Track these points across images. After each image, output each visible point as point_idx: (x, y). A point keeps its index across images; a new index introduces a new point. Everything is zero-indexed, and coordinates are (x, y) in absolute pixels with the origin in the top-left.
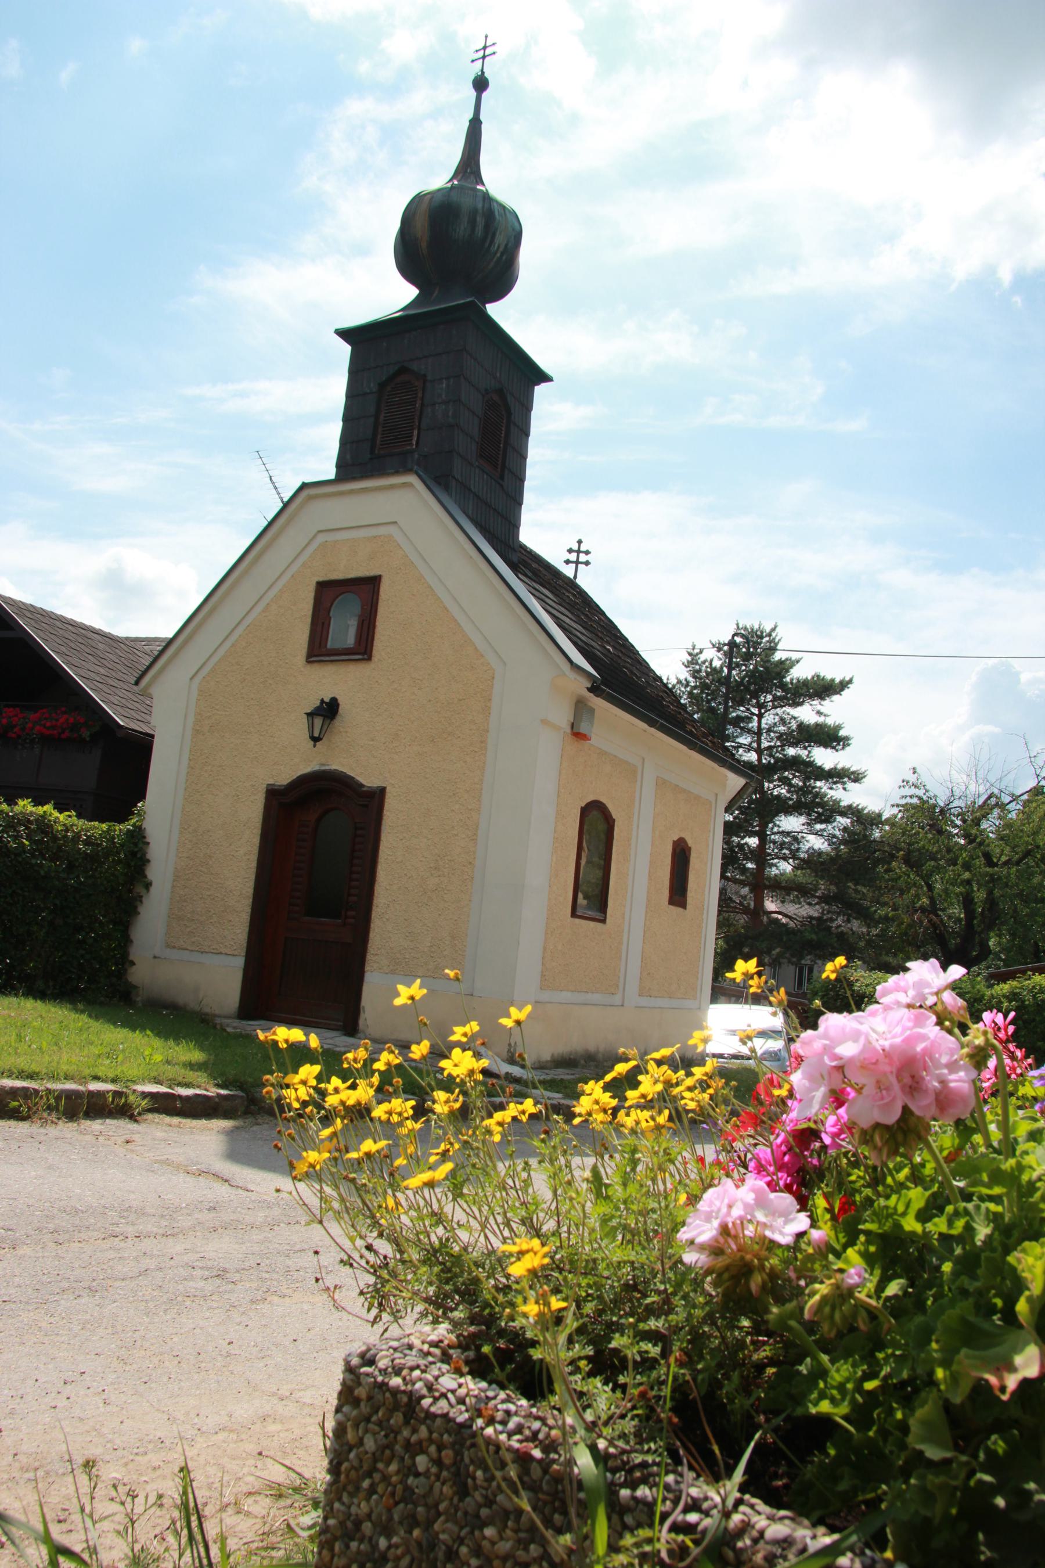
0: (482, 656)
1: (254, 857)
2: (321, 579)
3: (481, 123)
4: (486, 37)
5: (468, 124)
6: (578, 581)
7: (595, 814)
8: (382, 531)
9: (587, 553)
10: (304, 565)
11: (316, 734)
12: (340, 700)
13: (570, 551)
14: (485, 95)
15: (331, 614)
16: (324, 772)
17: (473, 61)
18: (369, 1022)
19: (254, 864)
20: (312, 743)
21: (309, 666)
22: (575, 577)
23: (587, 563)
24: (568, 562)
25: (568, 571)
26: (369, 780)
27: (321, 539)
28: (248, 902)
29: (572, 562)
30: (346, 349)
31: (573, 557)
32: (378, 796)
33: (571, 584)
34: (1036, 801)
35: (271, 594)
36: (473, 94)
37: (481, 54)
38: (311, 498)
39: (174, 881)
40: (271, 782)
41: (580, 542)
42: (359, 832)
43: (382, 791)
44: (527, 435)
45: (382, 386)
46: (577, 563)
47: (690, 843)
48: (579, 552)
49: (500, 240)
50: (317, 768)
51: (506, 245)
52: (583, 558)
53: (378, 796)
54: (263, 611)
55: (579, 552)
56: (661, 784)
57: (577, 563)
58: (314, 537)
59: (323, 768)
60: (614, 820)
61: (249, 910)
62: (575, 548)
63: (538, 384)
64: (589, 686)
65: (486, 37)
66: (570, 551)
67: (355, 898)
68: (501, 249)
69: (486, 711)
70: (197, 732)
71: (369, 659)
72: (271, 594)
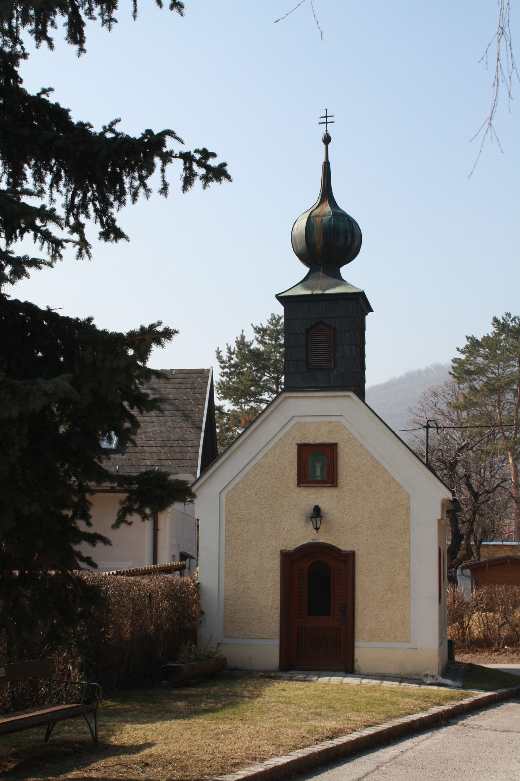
0: (401, 487)
2: (299, 442)
8: (333, 419)
10: (287, 433)
12: (320, 506)
14: (330, 145)
19: (278, 591)
20: (315, 531)
21: (298, 489)
26: (344, 546)
27: (295, 420)
28: (278, 610)
34: (471, 421)
36: (324, 146)
39: (225, 602)
40: (283, 548)
45: (307, 330)
49: (356, 244)
50: (311, 541)
53: (351, 556)
54: (264, 457)
69: (408, 514)
70: (228, 522)
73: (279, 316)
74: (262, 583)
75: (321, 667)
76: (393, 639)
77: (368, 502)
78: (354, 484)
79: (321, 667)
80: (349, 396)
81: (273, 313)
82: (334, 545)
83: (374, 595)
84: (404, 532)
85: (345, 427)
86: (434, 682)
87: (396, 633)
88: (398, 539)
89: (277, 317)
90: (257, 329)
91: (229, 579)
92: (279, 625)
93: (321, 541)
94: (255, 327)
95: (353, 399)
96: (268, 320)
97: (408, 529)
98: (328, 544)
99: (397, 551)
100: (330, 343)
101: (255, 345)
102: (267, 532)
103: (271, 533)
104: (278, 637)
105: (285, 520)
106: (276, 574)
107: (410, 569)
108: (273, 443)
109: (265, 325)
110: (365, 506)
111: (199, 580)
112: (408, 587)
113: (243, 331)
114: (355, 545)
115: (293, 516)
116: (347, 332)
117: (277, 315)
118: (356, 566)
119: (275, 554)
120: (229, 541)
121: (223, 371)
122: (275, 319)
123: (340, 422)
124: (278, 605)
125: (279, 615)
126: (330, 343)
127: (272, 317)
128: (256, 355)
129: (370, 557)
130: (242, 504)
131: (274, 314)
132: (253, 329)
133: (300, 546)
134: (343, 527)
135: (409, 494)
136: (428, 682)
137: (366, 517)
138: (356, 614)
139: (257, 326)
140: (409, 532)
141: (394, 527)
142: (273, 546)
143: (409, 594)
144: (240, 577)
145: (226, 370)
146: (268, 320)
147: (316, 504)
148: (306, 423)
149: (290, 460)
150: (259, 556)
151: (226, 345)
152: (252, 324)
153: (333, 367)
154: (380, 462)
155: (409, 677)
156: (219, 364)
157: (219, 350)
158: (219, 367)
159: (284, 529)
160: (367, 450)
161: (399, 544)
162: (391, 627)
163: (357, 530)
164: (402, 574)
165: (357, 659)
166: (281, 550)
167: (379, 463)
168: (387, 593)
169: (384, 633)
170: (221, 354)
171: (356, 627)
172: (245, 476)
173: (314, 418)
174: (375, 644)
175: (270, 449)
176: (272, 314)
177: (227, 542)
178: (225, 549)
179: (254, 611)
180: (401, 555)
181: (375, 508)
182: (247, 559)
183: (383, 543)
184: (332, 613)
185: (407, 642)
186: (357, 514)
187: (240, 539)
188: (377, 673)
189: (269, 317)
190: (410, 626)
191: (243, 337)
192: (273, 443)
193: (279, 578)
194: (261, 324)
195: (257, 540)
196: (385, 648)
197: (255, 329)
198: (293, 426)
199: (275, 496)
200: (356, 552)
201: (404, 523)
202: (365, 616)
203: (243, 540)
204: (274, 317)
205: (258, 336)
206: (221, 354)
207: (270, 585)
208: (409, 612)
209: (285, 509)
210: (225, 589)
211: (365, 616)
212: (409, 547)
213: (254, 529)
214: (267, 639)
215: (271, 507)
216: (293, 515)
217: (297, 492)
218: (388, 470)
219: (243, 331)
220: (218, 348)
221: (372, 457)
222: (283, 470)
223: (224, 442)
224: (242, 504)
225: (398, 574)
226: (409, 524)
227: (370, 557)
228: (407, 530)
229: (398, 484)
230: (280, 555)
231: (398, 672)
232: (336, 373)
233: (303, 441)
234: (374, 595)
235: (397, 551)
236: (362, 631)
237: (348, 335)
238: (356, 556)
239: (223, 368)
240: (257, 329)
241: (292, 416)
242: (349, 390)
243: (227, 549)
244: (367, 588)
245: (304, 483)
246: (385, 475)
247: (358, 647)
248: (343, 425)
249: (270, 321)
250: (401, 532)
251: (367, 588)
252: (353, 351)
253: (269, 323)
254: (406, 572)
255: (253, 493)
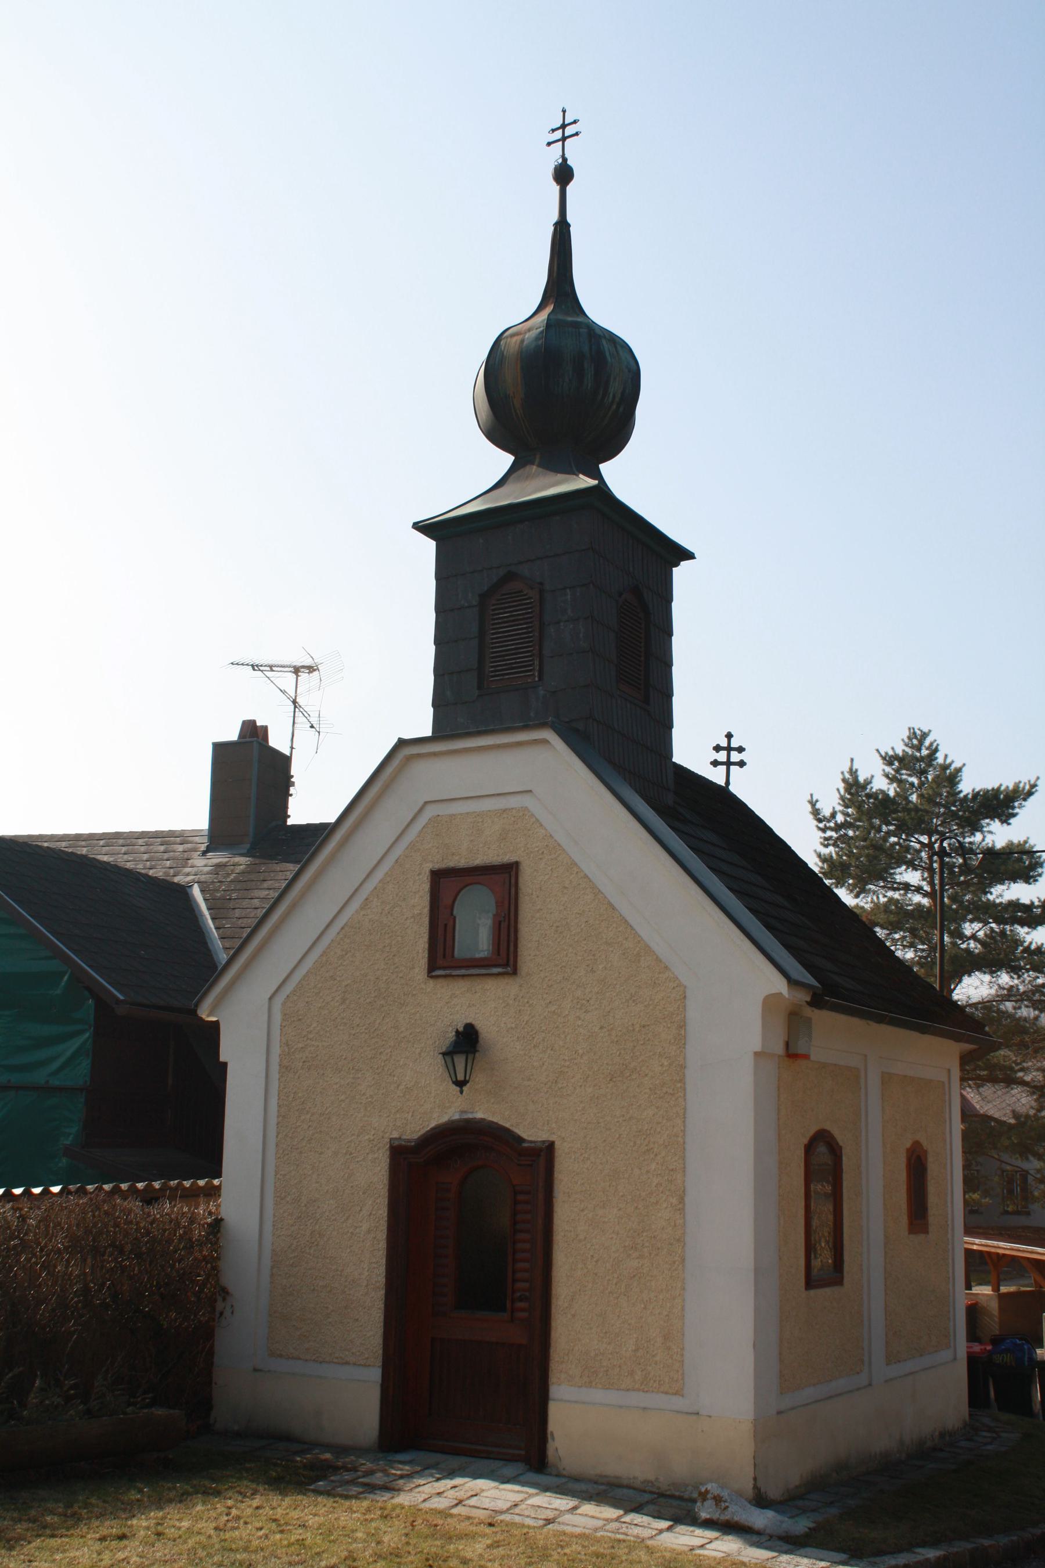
0: (666, 967)
1: (382, 1235)
2: (437, 866)
3: (569, 225)
4: (564, 111)
5: (552, 228)
6: (732, 788)
7: (822, 1149)
9: (741, 750)
10: (412, 846)
11: (460, 1077)
12: (479, 1025)
13: (717, 748)
14: (569, 188)
15: (455, 912)
16: (468, 1121)
17: (549, 144)
18: (561, 1452)
19: (383, 1245)
20: (458, 1089)
21: (431, 982)
22: (728, 782)
23: (742, 764)
24: (715, 763)
25: (717, 776)
26: (531, 1132)
27: (430, 812)
29: (722, 763)
30: (429, 546)
31: (722, 756)
32: (548, 1150)
33: (722, 796)
35: (370, 886)
36: (556, 188)
37: (558, 134)
38: (409, 759)
40: (395, 1135)
41: (729, 736)
42: (520, 1197)
43: (550, 1147)
44: (670, 634)
45: (484, 597)
46: (728, 764)
47: (925, 1144)
48: (729, 749)
49: (615, 388)
50: (457, 1117)
51: (623, 393)
52: (735, 757)
55: (729, 749)
56: (886, 1079)
57: (728, 764)
58: (421, 810)
59: (465, 1116)
60: (841, 1148)
61: (382, 1306)
62: (724, 744)
63: (677, 565)
64: (808, 999)
65: (564, 111)
66: (717, 748)
67: (526, 1285)
68: (617, 399)
69: (681, 1040)
70: (285, 1069)
71: (515, 972)
72: (370, 886)
73: (921, 731)
74: (350, 1221)
75: (479, 1447)
76: (642, 1384)
77: (586, 1012)
78: (556, 965)
79: (479, 1447)
80: (545, 742)
81: (912, 726)
82: (507, 1125)
83: (597, 1262)
84: (671, 1091)
85: (537, 820)
86: (715, 1516)
87: (650, 1368)
88: (657, 1108)
89: (918, 732)
90: (887, 759)
91: (281, 1211)
92: (380, 1331)
93: (479, 1115)
94: (883, 754)
95: (555, 748)
96: (903, 740)
97: (680, 1081)
98: (493, 1122)
99: (654, 1143)
100: (531, 622)
101: (880, 784)
102: (364, 1094)
103: (371, 1096)
104: (379, 1362)
105: (401, 1063)
106: (378, 1201)
107: (684, 1191)
108: (379, 874)
109: (900, 749)
110: (580, 1023)
111: (223, 1214)
112: (678, 1240)
113: (852, 760)
114: (554, 1125)
115: (420, 1054)
116: (568, 591)
117: (919, 729)
118: (556, 1182)
119: (378, 1150)
120: (284, 1117)
121: (823, 835)
122: (916, 738)
123: (526, 809)
124: (382, 1280)
125: (381, 1305)
126: (531, 622)
127: (910, 733)
128: (883, 806)
129: (588, 1159)
130: (315, 1025)
131: (913, 729)
132: (880, 758)
133: (432, 1129)
134: (529, 1080)
135: (685, 987)
136: (704, 1515)
137: (581, 1052)
138: (554, 1310)
139: (886, 753)
140: (685, 1090)
141: (646, 1075)
142: (375, 1129)
143: (683, 1260)
144: (306, 1205)
145: (829, 833)
146: (903, 740)
147: (468, 1021)
148: (452, 817)
149: (416, 912)
150: (346, 1154)
151: (836, 792)
152: (878, 750)
153: (537, 679)
154: (615, 905)
155: (677, 1494)
156: (815, 823)
157: (814, 800)
158: (815, 829)
159: (398, 1086)
160: (586, 876)
161: (658, 1123)
162: (636, 1350)
163: (560, 1086)
164: (665, 1205)
165: (552, 1433)
166: (391, 1139)
167: (614, 908)
168: (629, 1256)
169: (620, 1366)
170: (818, 806)
171: (553, 1344)
172: (322, 955)
173: (469, 802)
174: (598, 1395)
175: (375, 888)
176: (909, 729)
177: (281, 1118)
178: (277, 1137)
179: (330, 1291)
180: (663, 1154)
181: (601, 1028)
182: (320, 1162)
183: (621, 1120)
184: (508, 1305)
185: (676, 1394)
186: (561, 1043)
187: (308, 1112)
188: (601, 1476)
189: (905, 734)
190: (683, 1349)
191: (853, 773)
192: (379, 874)
193: (386, 1210)
194: (893, 748)
195: (342, 1112)
196: (621, 1407)
197: (884, 758)
198: (424, 827)
199: (382, 1002)
200: (557, 1145)
201: (670, 1064)
202: (574, 1316)
203: (313, 1114)
204: (914, 733)
205: (888, 769)
206: (818, 806)
207: (365, 1227)
208: (683, 1309)
209: (402, 1035)
210: (274, 1235)
211: (574, 1316)
212: (684, 1131)
213: (335, 1087)
214: (354, 1364)
215: (372, 1030)
216: (418, 1051)
217: (429, 990)
218: (635, 927)
219: (852, 760)
220: (812, 795)
221: (597, 892)
222: (399, 938)
223: (1012, 991)
224: (315, 1025)
225: (657, 1202)
226: (683, 1067)
227: (588, 1159)
228: (679, 1085)
229: (658, 960)
230: (388, 1153)
231: (652, 1478)
232: (542, 692)
233: (446, 861)
234: (597, 1262)
235: (654, 1143)
236: (566, 1358)
237: (569, 597)
238: (556, 1154)
239: (824, 830)
240: (887, 759)
241: (421, 803)
242: (542, 725)
243: (280, 1136)
244: (580, 1241)
245: (444, 968)
246: (626, 939)
247: (554, 1400)
248: (533, 815)
249: (906, 740)
250: (665, 1090)
251: (580, 1241)
252: (581, 635)
253: (906, 745)
254: (674, 1201)
255: (337, 999)
